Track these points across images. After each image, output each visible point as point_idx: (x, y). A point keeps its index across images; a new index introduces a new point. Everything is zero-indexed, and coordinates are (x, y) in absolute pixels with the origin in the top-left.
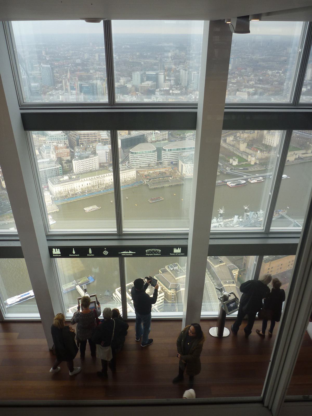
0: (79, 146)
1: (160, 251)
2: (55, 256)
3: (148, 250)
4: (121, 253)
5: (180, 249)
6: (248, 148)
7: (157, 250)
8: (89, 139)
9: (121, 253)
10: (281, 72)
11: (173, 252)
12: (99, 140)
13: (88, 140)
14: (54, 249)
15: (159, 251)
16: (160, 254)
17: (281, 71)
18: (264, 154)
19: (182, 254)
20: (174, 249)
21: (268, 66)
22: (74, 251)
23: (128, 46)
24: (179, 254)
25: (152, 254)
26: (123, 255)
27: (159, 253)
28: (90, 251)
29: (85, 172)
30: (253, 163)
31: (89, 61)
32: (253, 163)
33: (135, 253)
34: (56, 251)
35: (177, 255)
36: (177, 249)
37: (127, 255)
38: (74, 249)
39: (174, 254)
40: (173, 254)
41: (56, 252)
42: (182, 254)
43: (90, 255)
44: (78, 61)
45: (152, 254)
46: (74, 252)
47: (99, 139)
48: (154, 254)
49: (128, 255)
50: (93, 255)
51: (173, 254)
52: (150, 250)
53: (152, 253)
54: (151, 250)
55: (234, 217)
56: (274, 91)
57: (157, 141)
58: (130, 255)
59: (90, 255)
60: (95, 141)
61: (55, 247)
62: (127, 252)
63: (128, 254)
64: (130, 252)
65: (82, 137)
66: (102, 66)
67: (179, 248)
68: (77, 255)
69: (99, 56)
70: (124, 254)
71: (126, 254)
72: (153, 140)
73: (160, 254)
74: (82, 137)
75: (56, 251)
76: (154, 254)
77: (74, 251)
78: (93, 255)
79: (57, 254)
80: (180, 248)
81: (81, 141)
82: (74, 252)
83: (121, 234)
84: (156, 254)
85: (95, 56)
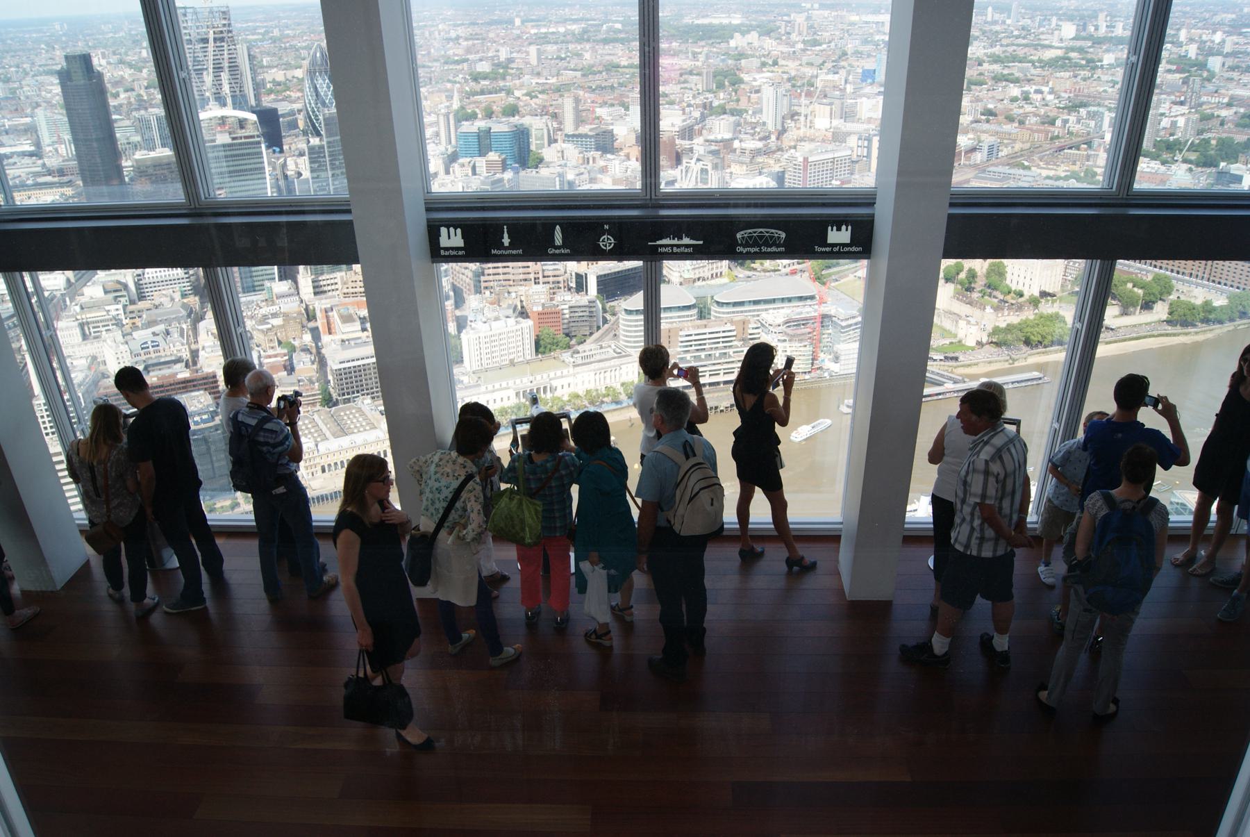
0: (480, 293)
1: (783, 235)
2: (447, 253)
3: (742, 232)
4: (659, 243)
5: (847, 230)
6: (958, 299)
7: (773, 231)
8: (509, 273)
9: (659, 243)
10: (1046, 89)
11: (824, 243)
12: (535, 279)
13: (506, 277)
14: (443, 230)
15: (779, 238)
16: (782, 249)
17: (1048, 86)
18: (1003, 316)
19: (854, 249)
20: (830, 228)
21: (1009, 74)
22: (506, 235)
23: (619, 26)
24: (846, 249)
25: (757, 250)
26: (663, 250)
27: (778, 246)
28: (558, 238)
29: (495, 365)
30: (971, 342)
31: (512, 65)
32: (971, 342)
33: (701, 242)
34: (449, 238)
35: (839, 253)
36: (839, 229)
37: (675, 250)
38: (505, 230)
39: (828, 249)
40: (824, 249)
41: (452, 239)
42: (854, 249)
43: (557, 251)
44: (484, 67)
45: (757, 250)
46: (506, 241)
47: (537, 276)
48: (764, 249)
49: (678, 250)
50: (567, 251)
51: (824, 249)
52: (750, 231)
53: (755, 244)
54: (755, 232)
55: (918, 500)
56: (1027, 142)
57: (699, 279)
58: (686, 251)
59: (557, 251)
60: (526, 280)
61: (449, 224)
62: (676, 242)
63: (678, 246)
64: (686, 241)
65: (489, 268)
66: (546, 79)
67: (844, 227)
68: (514, 252)
69: (539, 53)
70: (666, 246)
71: (672, 246)
72: (686, 276)
73: (782, 249)
74: (489, 268)
75: (449, 238)
76: (764, 249)
77: (506, 235)
78: (567, 251)
79: (452, 249)
80: (850, 228)
81: (486, 281)
82: (506, 241)
83: (653, 197)
84: (769, 250)
85: (528, 53)
